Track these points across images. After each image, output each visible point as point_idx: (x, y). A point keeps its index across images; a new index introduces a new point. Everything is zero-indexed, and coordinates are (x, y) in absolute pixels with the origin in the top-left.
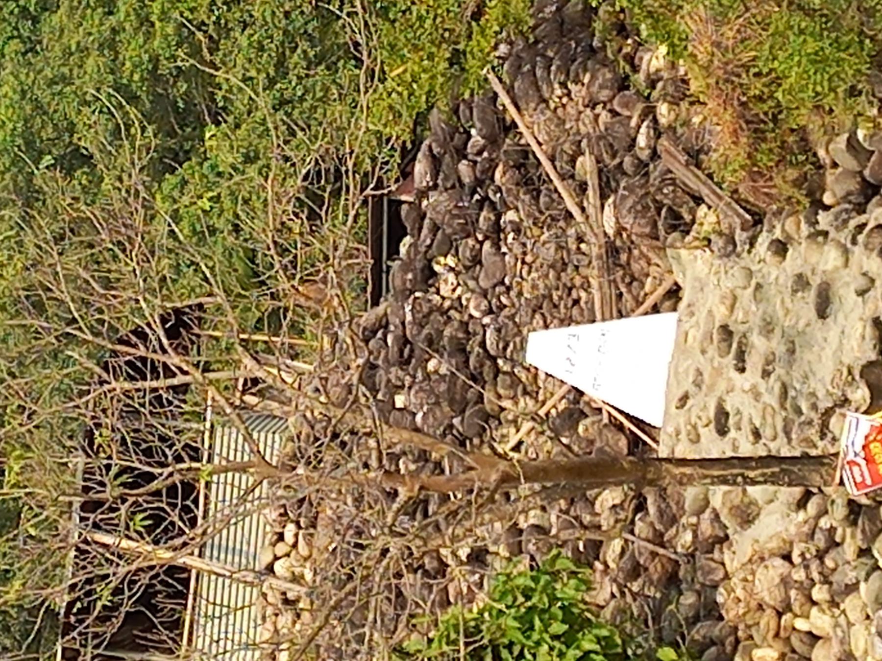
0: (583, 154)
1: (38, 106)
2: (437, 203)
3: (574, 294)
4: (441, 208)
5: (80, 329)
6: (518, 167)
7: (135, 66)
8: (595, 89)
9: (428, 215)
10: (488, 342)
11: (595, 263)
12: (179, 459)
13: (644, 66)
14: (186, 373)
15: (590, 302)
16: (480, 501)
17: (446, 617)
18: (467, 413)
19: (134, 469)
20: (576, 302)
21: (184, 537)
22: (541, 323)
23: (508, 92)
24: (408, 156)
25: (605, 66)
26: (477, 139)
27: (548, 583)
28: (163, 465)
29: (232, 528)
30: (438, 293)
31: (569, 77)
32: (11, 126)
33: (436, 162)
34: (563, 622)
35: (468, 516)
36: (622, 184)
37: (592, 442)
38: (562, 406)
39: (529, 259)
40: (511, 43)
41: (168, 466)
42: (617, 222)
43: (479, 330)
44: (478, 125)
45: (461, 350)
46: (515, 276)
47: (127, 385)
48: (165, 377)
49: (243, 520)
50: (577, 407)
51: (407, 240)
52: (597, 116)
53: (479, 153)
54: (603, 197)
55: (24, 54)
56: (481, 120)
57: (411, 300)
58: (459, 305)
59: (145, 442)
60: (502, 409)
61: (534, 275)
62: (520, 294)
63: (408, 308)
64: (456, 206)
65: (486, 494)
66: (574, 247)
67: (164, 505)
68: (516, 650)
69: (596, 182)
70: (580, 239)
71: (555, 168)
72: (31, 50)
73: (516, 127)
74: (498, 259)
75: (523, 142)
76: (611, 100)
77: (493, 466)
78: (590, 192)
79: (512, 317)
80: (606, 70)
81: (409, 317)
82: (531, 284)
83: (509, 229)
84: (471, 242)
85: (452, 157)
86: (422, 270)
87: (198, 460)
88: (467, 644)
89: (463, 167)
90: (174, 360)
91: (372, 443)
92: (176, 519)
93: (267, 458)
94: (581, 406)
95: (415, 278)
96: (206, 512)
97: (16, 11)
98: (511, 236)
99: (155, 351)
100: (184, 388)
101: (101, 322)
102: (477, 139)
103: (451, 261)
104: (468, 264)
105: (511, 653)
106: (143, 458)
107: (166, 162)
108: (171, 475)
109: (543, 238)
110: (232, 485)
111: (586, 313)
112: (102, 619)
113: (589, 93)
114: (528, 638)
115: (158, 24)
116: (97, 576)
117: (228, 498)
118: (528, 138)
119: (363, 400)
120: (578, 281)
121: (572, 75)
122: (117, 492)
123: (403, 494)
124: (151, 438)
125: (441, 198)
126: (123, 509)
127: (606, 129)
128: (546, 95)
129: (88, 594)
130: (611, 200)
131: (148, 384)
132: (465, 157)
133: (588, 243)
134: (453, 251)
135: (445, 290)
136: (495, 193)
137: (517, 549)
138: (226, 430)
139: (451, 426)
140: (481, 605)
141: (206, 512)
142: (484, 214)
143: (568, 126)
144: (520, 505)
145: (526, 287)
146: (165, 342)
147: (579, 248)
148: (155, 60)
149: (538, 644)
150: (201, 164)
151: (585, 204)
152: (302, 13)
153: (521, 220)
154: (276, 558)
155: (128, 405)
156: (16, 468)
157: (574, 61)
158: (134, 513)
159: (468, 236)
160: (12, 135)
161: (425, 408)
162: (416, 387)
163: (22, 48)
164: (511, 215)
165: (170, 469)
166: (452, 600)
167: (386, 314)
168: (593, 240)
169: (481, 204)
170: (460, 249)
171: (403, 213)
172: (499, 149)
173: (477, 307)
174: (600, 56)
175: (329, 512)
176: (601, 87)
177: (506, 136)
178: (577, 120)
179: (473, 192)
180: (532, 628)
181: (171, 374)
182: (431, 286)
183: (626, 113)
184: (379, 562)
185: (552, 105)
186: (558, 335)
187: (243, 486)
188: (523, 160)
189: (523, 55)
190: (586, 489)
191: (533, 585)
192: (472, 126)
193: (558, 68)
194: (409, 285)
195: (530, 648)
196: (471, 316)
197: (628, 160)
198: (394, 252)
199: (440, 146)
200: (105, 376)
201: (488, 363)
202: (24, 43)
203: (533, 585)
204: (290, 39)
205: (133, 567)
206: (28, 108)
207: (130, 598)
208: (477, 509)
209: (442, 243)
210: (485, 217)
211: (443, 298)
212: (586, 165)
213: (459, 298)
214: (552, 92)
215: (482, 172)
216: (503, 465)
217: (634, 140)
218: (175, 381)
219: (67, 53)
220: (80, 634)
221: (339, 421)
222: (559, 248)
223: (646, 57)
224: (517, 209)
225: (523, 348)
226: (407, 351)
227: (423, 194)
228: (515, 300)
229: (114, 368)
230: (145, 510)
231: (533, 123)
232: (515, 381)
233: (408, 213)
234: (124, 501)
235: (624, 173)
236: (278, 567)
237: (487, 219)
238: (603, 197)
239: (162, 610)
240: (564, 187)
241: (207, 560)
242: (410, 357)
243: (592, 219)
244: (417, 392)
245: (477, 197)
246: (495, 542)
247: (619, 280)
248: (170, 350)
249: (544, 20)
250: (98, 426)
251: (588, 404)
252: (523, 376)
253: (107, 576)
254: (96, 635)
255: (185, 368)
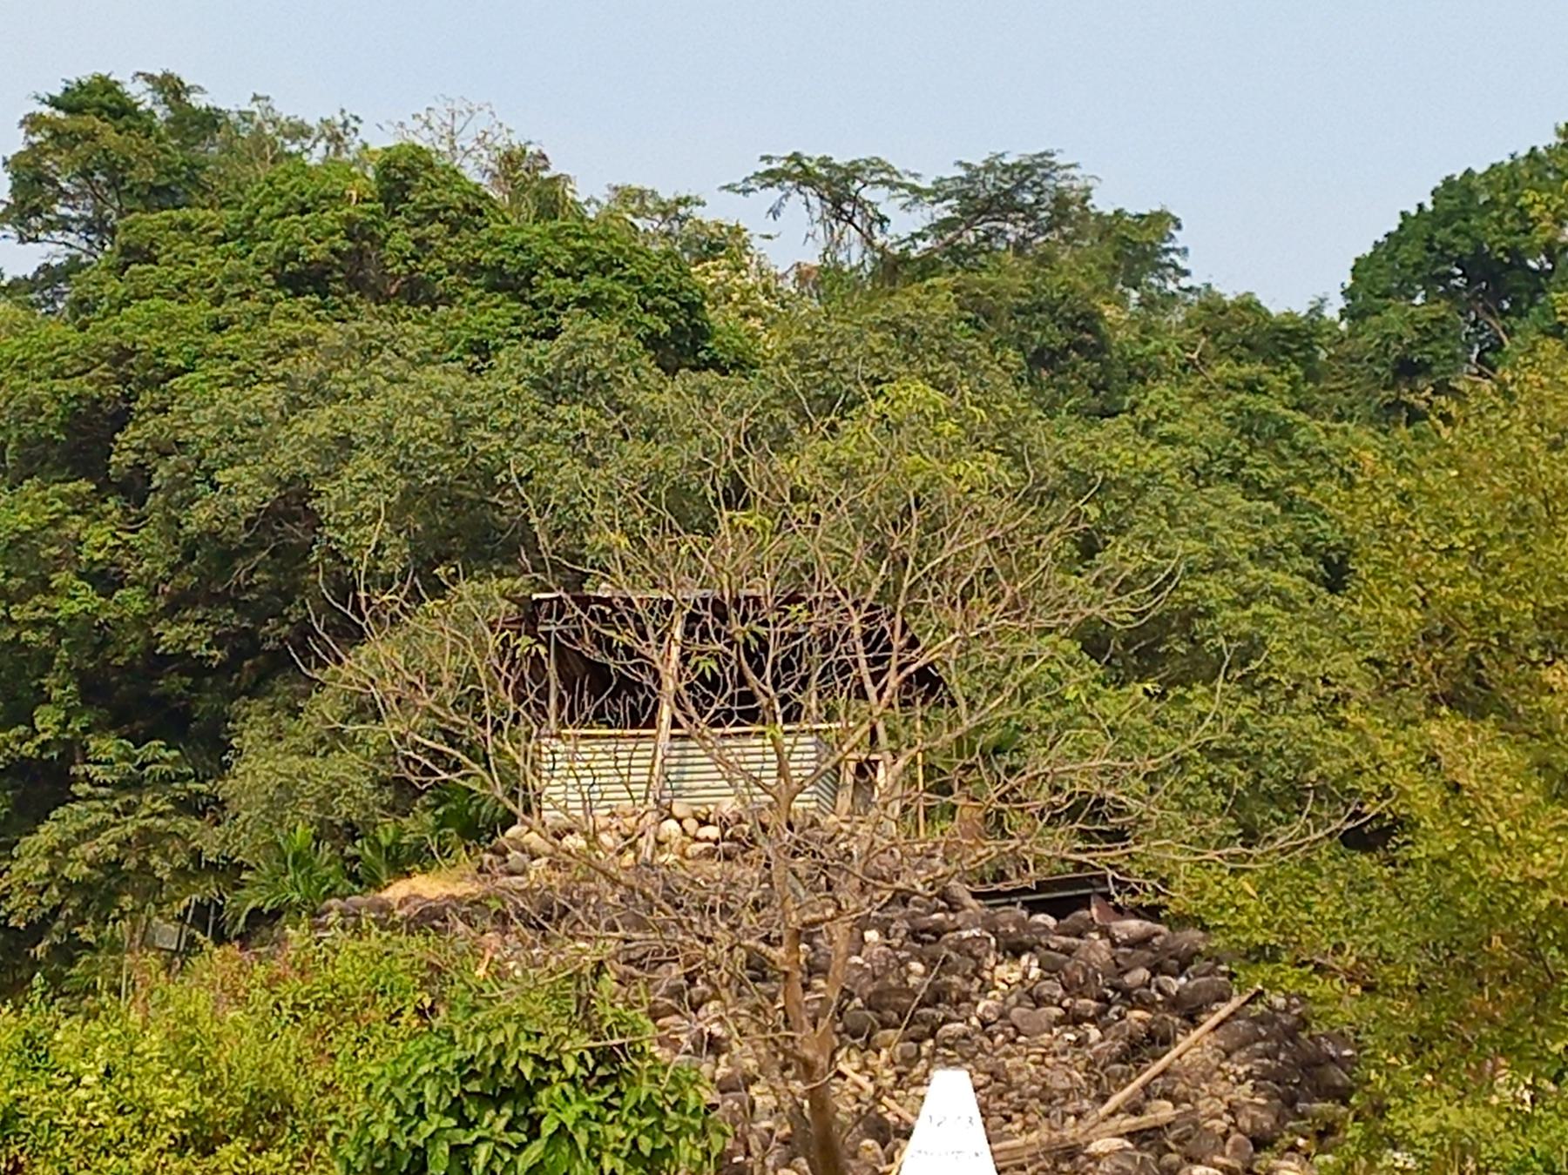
0: (1175, 1107)
1: (1141, 491)
2: (1097, 949)
3: (1016, 1116)
4: (1093, 955)
5: (913, 574)
6: (1151, 1035)
7: (1200, 593)
8: (1250, 1110)
9: (1083, 942)
10: (950, 1026)
11: (1055, 1135)
12: (784, 700)
13: (1285, 1163)
14: (880, 694)
15: (1011, 1135)
16: (781, 1041)
17: (642, 1018)
18: (868, 1013)
19: (766, 652)
20: (1008, 1119)
21: (696, 717)
22: (981, 1083)
23: (1233, 1014)
24: (1152, 913)
25: (1278, 1120)
26: (1175, 984)
27: (693, 1127)
28: (776, 683)
29: (713, 768)
30: (997, 963)
31: (1259, 1080)
32: (1115, 465)
33: (1143, 942)
34: (653, 1150)
35: (762, 1029)
36: (1148, 1156)
37: (855, 1156)
38: (889, 1117)
39: (1049, 1060)
40: (1287, 1010)
41: (776, 690)
42: (1105, 1155)
43: (963, 1013)
44: (1191, 985)
45: (937, 996)
46: (1028, 1047)
47: (857, 632)
48: (872, 675)
49: (723, 778)
50: (893, 1135)
51: (1051, 921)
52: (1219, 1117)
53: (1160, 990)
54: (1130, 1135)
55: (1192, 468)
56: (1197, 989)
57: (985, 934)
58: (984, 990)
59: (799, 661)
60: (878, 1052)
61: (1032, 1068)
62: (1008, 1055)
63: (976, 932)
64: (1096, 971)
65: (789, 1046)
66: (1069, 1108)
67: (729, 691)
68: (616, 1101)
69: (1146, 1126)
70: (1079, 1115)
71: (1156, 1077)
72: (1198, 475)
73: (1196, 1027)
74: (1045, 1026)
75: (1179, 1037)
76: (1239, 1131)
77: (821, 1050)
78: (1133, 1120)
79: (981, 1049)
80: (1273, 1120)
81: (965, 934)
82: (1022, 1066)
83: (1081, 1034)
84: (1059, 992)
85: (1151, 960)
86: (1020, 943)
87: (786, 720)
88: (621, 1046)
89: (1142, 974)
90: (893, 680)
91: (830, 912)
92: (716, 706)
93: (799, 797)
94: (894, 1140)
95: (1011, 935)
96: (728, 736)
97: (1239, 454)
98: (1072, 1037)
99: (899, 658)
100: (862, 694)
101: (924, 595)
102: (1175, 984)
103: (1035, 972)
104: (1035, 992)
105: (612, 1096)
106: (780, 661)
107: (1094, 641)
108: (767, 695)
109: (1075, 1074)
110: (765, 761)
111: (998, 1132)
112: (598, 640)
113: (1244, 1105)
114: (630, 1113)
115: (1248, 613)
116: (644, 627)
117: (748, 758)
118: (1184, 1042)
119: (876, 896)
120: (1031, 1118)
121: (1261, 1083)
122: (739, 637)
123: (778, 953)
124: (804, 666)
125: (1103, 954)
126: (720, 646)
127: (1207, 1129)
128: (1235, 1057)
129: (621, 619)
130: (1128, 1145)
131: (862, 657)
132: (1153, 975)
133: (1075, 1126)
134: (1046, 974)
135: (1001, 971)
136: (1119, 1013)
137: (725, 1087)
138: (812, 748)
139: (851, 996)
140: (658, 1055)
141: (728, 736)
142: (1094, 1004)
143: (1204, 1086)
144: (780, 1086)
145: (1018, 1061)
146: (912, 668)
147: (1069, 1114)
148: (1209, 613)
149: (625, 1125)
150: (1097, 679)
151: (1120, 1116)
152: (1283, 770)
153: (1091, 1046)
154: (680, 821)
155: (836, 638)
156: (751, 523)
157: (1278, 1083)
158: (717, 658)
159: (1065, 988)
160: (1105, 466)
161: (868, 965)
162: (890, 952)
163: (1198, 465)
164: (1094, 1034)
165: (772, 693)
166: (660, 1022)
167: (964, 908)
168: (1081, 1130)
169: (1103, 998)
170: (1049, 982)
171: (1080, 913)
172: (1169, 1011)
173: (986, 1009)
174: (1287, 1111)
175: (738, 873)
176: (1253, 1118)
177: (1184, 1017)
178: (1212, 1095)
179: (1115, 989)
180: (642, 1115)
181: (876, 678)
182: (1004, 955)
183: (1228, 1150)
184: (701, 938)
185: (1225, 1065)
186: (969, 1104)
187: (764, 774)
188: (1157, 1040)
189: (1276, 1026)
190: (807, 1157)
191: (689, 1110)
192: (1189, 979)
193: (1269, 1067)
194: (1001, 929)
195: (619, 1116)
196: (977, 1004)
197: (1175, 1158)
198: (1034, 908)
199: (1162, 944)
200: (864, 606)
201: (927, 1029)
202: (1204, 468)
203: (689, 1110)
204: (1250, 760)
205: (659, 666)
206: (1135, 482)
207: (624, 666)
208: (772, 1039)
209: (1054, 961)
210: (1089, 1005)
211: (992, 970)
212: (1163, 1111)
213: (996, 988)
214: (1239, 1064)
215: (1138, 996)
216: (823, 1061)
217: (1199, 1162)
218: (868, 685)
219: (1200, 517)
220: (579, 617)
221: (849, 872)
222: (1066, 1093)
223: (1293, 1165)
224: (1102, 1040)
225: (948, 1065)
226: (927, 936)
227: (1105, 932)
228: (1002, 1050)
229: (876, 616)
230: (722, 670)
231: (1202, 1046)
232: (910, 1061)
233: (1080, 918)
234: (730, 646)
235: (1160, 1156)
236: (671, 825)
237: (1087, 1008)
238: (1130, 1135)
239: (616, 704)
240: (1135, 1090)
241: (668, 745)
242: (923, 942)
243: (1104, 1126)
244: (885, 954)
245: (1111, 993)
246: (728, 1063)
247: (1040, 1164)
248: (903, 675)
249: (1318, 1044)
250: (810, 608)
251: (897, 1146)
252: (918, 1070)
253: (645, 638)
254: (579, 635)
255: (886, 695)
